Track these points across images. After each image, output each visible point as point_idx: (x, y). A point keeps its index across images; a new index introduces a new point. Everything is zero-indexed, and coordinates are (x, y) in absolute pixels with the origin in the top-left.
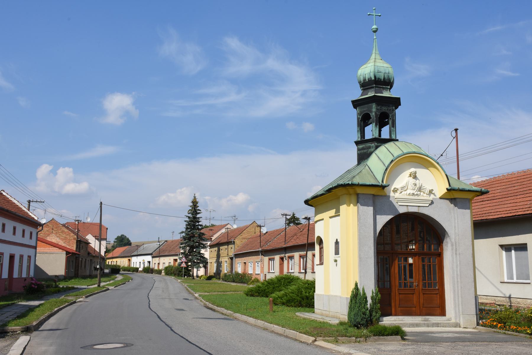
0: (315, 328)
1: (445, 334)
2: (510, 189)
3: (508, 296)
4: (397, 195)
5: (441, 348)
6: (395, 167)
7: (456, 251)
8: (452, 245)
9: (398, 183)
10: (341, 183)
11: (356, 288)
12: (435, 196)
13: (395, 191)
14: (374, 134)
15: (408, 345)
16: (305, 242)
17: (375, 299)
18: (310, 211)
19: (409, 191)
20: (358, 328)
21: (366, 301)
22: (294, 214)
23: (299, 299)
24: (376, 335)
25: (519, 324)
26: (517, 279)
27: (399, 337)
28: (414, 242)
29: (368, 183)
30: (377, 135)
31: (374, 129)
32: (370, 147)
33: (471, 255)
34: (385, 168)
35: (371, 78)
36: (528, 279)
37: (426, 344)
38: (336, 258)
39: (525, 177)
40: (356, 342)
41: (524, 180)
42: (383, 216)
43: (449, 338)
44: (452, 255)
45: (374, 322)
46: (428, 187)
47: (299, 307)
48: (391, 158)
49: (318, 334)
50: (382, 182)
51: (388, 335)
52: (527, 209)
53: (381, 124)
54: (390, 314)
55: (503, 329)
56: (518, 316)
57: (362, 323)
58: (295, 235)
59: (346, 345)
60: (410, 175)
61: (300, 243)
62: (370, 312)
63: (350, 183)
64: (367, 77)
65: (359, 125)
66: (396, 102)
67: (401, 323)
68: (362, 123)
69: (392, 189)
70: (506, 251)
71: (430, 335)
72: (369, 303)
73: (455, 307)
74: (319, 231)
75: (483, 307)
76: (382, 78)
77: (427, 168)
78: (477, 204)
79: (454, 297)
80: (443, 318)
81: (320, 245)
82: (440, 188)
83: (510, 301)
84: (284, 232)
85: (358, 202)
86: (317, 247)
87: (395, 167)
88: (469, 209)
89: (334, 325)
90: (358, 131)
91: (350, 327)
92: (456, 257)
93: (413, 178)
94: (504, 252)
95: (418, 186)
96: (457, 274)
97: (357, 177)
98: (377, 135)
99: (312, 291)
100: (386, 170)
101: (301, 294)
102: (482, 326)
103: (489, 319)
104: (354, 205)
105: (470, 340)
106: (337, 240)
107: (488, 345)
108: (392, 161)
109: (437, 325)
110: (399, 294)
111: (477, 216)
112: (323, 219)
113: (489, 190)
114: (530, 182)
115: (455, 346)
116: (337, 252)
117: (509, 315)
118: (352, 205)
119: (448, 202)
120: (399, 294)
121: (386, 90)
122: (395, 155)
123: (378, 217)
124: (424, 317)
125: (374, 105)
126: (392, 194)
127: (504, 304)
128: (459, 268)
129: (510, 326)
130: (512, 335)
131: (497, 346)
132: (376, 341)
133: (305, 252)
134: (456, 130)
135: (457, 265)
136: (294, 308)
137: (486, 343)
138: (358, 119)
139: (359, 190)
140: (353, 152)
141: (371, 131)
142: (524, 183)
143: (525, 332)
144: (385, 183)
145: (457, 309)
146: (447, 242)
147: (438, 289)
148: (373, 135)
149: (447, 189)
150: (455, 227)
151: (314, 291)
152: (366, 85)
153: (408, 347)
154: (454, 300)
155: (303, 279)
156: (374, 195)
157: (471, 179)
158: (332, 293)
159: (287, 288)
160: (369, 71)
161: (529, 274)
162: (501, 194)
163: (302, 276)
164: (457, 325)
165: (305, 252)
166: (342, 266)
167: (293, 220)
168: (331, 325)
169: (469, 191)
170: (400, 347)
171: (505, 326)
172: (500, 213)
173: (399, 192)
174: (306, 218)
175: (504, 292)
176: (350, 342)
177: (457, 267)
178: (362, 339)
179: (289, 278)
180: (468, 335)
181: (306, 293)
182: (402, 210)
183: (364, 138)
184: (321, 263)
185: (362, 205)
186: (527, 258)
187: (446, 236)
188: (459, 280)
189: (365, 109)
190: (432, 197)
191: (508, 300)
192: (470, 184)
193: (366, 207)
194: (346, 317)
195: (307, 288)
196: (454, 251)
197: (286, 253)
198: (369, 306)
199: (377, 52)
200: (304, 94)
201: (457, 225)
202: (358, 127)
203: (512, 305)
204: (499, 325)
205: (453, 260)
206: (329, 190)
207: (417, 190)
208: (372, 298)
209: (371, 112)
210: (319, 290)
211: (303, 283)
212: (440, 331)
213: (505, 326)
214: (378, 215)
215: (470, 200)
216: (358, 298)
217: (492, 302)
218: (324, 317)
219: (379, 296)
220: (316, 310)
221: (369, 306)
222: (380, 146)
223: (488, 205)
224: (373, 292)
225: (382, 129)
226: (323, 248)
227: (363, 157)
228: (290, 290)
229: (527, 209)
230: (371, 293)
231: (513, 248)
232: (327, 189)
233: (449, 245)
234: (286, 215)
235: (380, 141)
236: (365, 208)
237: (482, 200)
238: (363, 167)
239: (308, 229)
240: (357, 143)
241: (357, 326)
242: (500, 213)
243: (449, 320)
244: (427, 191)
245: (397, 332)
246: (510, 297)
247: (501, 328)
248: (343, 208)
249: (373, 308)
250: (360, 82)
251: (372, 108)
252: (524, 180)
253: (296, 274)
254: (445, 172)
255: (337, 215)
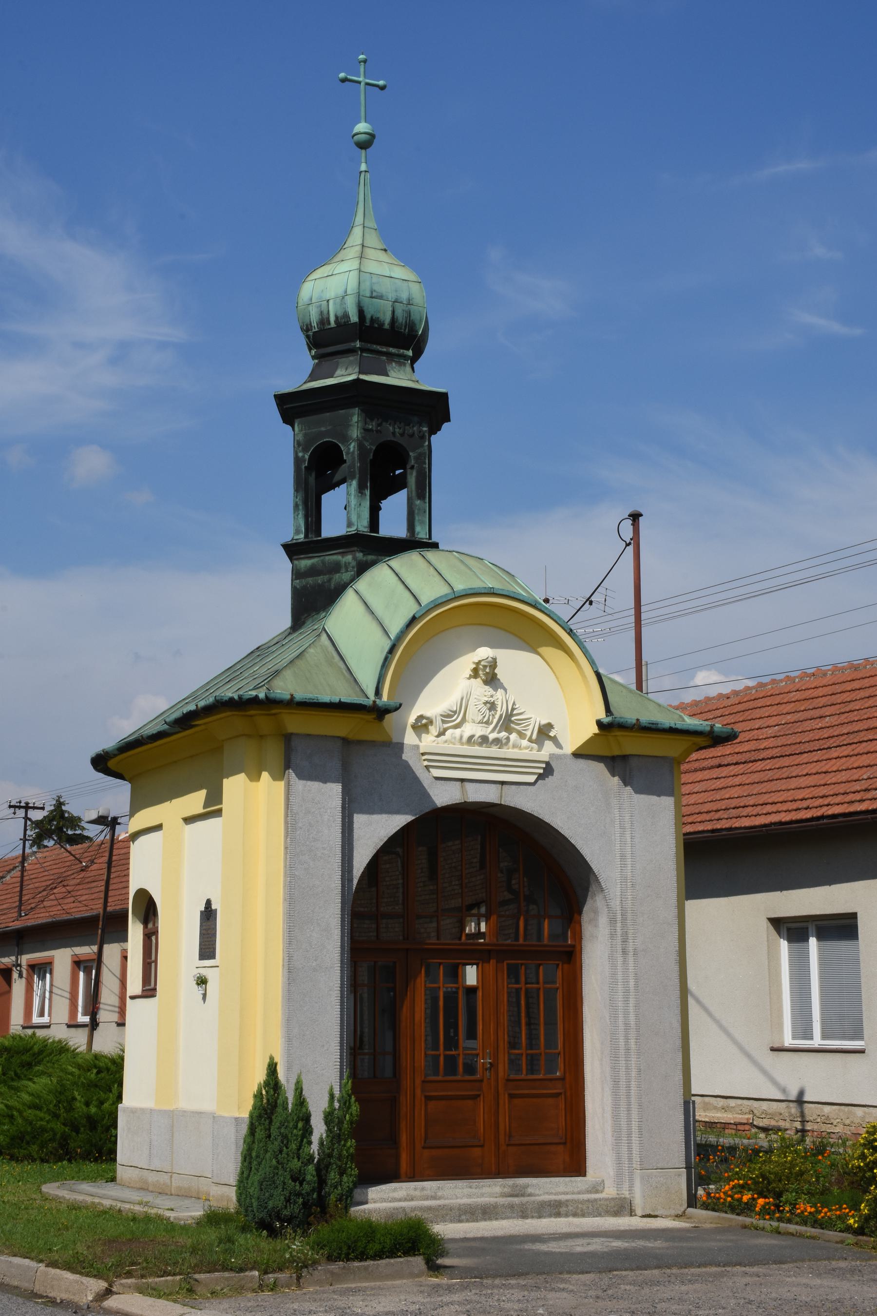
0: (111, 1242)
1: (580, 1241)
2: (808, 725)
3: (793, 1095)
4: (428, 742)
5: (563, 1295)
6: (420, 644)
7: (625, 941)
8: (612, 921)
9: (432, 702)
10: (229, 694)
11: (272, 1081)
12: (558, 745)
13: (422, 726)
14: (354, 518)
15: (450, 1289)
16: (97, 908)
17: (341, 1122)
18: (115, 796)
19: (468, 730)
20: (273, 1233)
21: (308, 1131)
22: (59, 804)
23: (58, 1127)
24: (338, 1258)
25: (821, 1196)
26: (824, 1037)
27: (418, 1262)
28: (483, 910)
29: (326, 698)
30: (362, 525)
31: (353, 502)
32: (336, 568)
33: (673, 957)
34: (387, 645)
35: (346, 315)
36: (858, 1035)
37: (513, 1282)
38: (204, 972)
39: (856, 685)
40: (261, 1288)
41: (853, 696)
42: (376, 817)
43: (592, 1255)
44: (611, 957)
45: (331, 1209)
46: (534, 716)
47: (61, 1159)
48: (409, 609)
49: (119, 1264)
50: (378, 692)
51: (379, 1255)
52: (858, 797)
53: (380, 487)
54: (389, 1175)
55: (771, 1214)
56: (823, 1167)
57: (286, 1213)
58: (61, 881)
59: (225, 1304)
60: (475, 673)
61: (77, 911)
62: (318, 1169)
63: (262, 695)
64: (333, 311)
65: (301, 484)
66: (433, 409)
67: (430, 1209)
68: (312, 479)
69: (412, 719)
70: (790, 941)
71: (528, 1246)
72: (315, 1138)
73: (617, 1140)
74: (146, 868)
75: (712, 1139)
76: (387, 319)
77: (532, 647)
78: (700, 776)
79: (616, 1107)
80: (577, 1182)
81: (145, 922)
82: (577, 719)
83: (802, 1115)
84: (17, 873)
85: (287, 766)
86: (135, 931)
87: (420, 644)
88: (670, 793)
89: (185, 1228)
90: (296, 506)
91: (244, 1229)
92: (625, 962)
93: (486, 682)
94: (784, 944)
95: (501, 710)
96: (627, 1025)
97: (288, 674)
98: (362, 525)
99: (112, 1097)
100: (392, 650)
101: (70, 1109)
102: (706, 1206)
103: (730, 1179)
104: (275, 778)
105: (659, 1262)
106: (208, 903)
107: (722, 1275)
108: (413, 620)
109: (556, 1209)
110: (428, 1098)
111: (700, 818)
112: (159, 827)
113: (737, 728)
114: (870, 702)
115: (610, 1287)
116: (207, 950)
117: (793, 1165)
118: (265, 775)
119: (600, 768)
120: (428, 1098)
121: (401, 364)
122: (425, 600)
123: (359, 820)
124: (510, 1182)
125: (355, 416)
126: (410, 738)
127: (782, 1124)
128: (632, 1001)
129: (794, 1205)
130: (800, 1235)
131: (748, 1279)
132: (335, 1278)
133: (95, 948)
134: (635, 517)
135: (627, 992)
136: (37, 1166)
137: (714, 1269)
138: (298, 461)
139: (295, 723)
140: (277, 582)
141: (342, 510)
142: (852, 706)
143: (840, 1225)
144: (385, 697)
145: (625, 1149)
146: (596, 912)
147: (562, 1079)
148: (350, 524)
149: (599, 723)
150: (623, 857)
151: (119, 1098)
152: (329, 339)
153: (446, 1299)
154: (616, 1117)
155: (83, 1048)
156: (346, 741)
157: (691, 680)
158: (183, 1104)
159: (17, 1089)
160: (340, 292)
161: (861, 1021)
162: (780, 741)
163: (78, 1040)
164: (623, 1207)
165: (95, 948)
166: (216, 1012)
167: (57, 826)
168: (171, 1227)
169: (673, 731)
170: (420, 1298)
171: (777, 1206)
172: (774, 808)
173: (434, 730)
174: (100, 820)
175: (782, 1080)
176: (239, 1290)
177: (626, 1000)
178: (283, 1276)
179: (27, 1050)
180: (658, 1244)
181: (87, 1104)
182: (443, 796)
183: (319, 533)
184: (149, 992)
185: (301, 776)
186: (856, 961)
187: (593, 887)
188: (632, 1042)
189: (323, 426)
190: (548, 750)
191: (794, 1109)
192: (682, 707)
193: (315, 785)
194: (232, 1193)
195: (93, 1085)
196: (619, 939)
197: (21, 953)
198: (315, 1147)
199: (372, 223)
200: (121, 354)
201: (628, 849)
202: (297, 490)
203: (808, 1127)
204: (761, 1201)
205: (614, 975)
206: (186, 721)
207: (496, 722)
208: (328, 1118)
209: (346, 439)
210: (137, 1093)
211: (79, 1067)
212: (566, 1230)
213: (777, 1206)
214: (362, 811)
215: (673, 763)
216: (277, 1120)
217: (743, 1118)
218: (149, 1198)
219: (355, 1108)
220: (121, 1172)
221: (315, 1147)
222: (373, 563)
223: (737, 780)
224: (332, 1096)
225: (385, 504)
226: (155, 932)
227: (312, 601)
228: (26, 1097)
229: (858, 797)
230: (326, 1098)
231: (812, 929)
232: (178, 714)
233: (603, 920)
234: (27, 807)
235: (374, 548)
236: (315, 786)
237: (716, 762)
238: (311, 639)
239: (110, 863)
240: (292, 550)
241: (269, 1225)
242: (774, 808)
243: (596, 1188)
244: (531, 730)
245: (411, 1241)
246: (800, 1101)
247: (765, 1212)
248: (234, 786)
249: (330, 1156)
250: (306, 329)
251: (347, 425)
252: (853, 696)
253: (59, 1033)
254: (592, 663)
255: (213, 809)
